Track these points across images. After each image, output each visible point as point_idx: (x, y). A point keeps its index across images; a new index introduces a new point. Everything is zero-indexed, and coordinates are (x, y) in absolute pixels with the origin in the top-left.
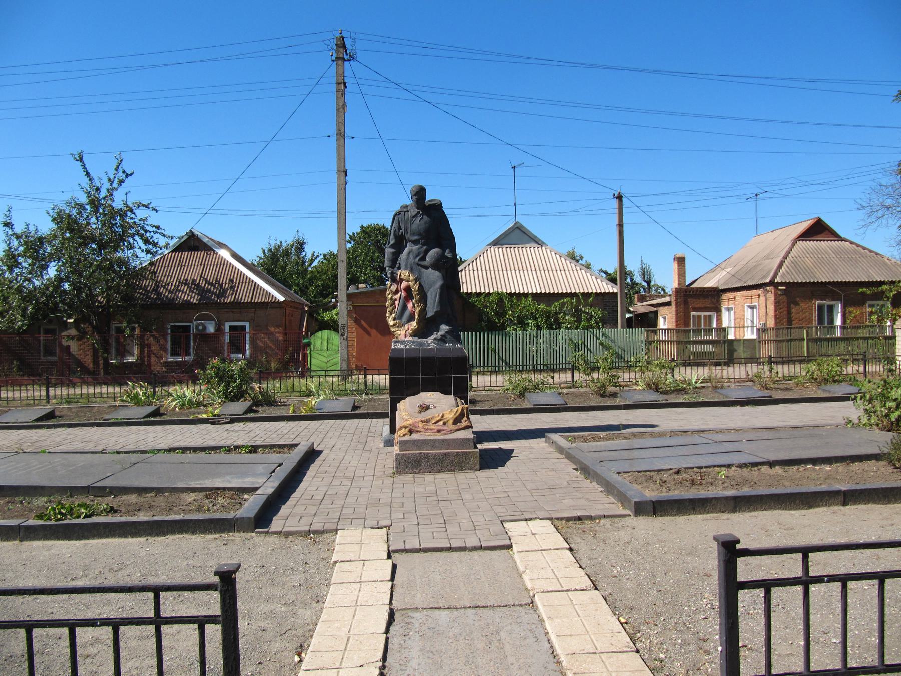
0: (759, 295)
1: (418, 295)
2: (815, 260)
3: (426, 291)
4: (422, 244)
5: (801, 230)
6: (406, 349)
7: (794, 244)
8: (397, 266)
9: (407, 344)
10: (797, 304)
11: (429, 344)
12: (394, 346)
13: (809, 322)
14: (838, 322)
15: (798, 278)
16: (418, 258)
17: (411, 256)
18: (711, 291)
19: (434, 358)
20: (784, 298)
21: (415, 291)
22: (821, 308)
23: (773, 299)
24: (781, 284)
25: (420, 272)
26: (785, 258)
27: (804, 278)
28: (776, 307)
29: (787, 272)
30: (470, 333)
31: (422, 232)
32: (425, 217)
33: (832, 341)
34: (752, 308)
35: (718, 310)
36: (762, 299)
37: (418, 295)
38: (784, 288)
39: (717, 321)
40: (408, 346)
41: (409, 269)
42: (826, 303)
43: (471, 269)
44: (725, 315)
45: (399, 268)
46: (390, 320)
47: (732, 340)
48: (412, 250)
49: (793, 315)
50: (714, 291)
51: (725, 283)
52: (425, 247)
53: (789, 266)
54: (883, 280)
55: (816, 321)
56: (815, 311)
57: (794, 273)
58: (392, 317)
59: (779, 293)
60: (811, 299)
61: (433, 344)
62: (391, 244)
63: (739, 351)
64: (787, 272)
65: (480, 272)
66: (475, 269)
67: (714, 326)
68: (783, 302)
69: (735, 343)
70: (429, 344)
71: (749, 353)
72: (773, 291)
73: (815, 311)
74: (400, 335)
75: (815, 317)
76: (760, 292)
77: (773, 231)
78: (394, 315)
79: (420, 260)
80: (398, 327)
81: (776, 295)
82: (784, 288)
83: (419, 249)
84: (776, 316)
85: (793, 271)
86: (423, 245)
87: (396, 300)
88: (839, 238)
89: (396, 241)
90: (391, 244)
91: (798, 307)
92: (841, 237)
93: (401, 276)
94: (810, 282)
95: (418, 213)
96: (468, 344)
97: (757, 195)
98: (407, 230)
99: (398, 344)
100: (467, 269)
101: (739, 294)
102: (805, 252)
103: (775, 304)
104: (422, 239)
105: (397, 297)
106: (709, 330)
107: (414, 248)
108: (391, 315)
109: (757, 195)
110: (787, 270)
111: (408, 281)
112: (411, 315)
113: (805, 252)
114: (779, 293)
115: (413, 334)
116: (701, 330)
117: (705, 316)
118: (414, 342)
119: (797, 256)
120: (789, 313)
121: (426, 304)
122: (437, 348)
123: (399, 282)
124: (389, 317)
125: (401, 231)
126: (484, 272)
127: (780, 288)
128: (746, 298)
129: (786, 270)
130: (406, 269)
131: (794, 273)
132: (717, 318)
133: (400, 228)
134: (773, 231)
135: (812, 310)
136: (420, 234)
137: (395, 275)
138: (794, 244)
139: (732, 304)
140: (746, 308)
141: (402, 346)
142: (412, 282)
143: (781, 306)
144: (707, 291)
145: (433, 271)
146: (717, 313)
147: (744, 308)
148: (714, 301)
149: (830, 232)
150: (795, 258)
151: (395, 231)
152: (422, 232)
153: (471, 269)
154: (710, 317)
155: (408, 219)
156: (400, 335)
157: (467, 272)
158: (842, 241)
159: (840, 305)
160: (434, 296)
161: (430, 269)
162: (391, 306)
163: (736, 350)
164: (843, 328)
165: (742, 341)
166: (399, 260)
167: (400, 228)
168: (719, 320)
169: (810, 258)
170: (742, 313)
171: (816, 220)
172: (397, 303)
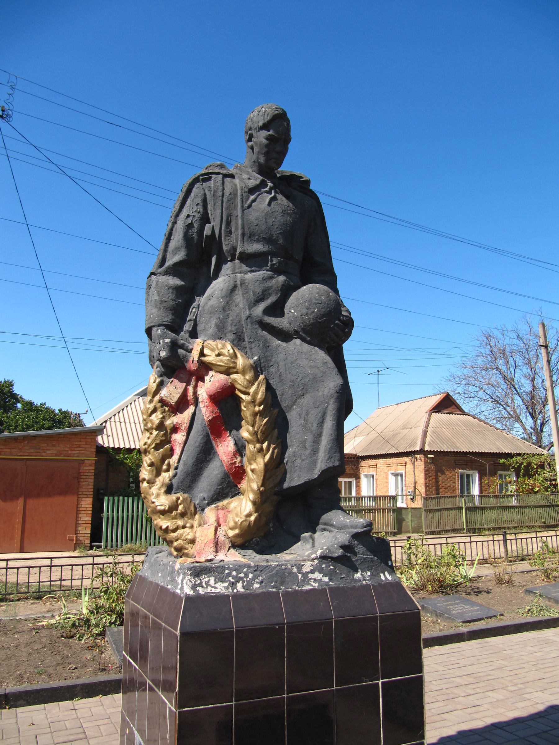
0: (406, 463)
1: (262, 414)
2: (451, 431)
3: (283, 405)
4: (273, 269)
5: (433, 403)
6: (237, 597)
7: (430, 416)
8: (187, 327)
9: (238, 579)
10: (443, 473)
11: (305, 575)
12: (194, 587)
13: (453, 491)
14: (475, 491)
15: (443, 447)
16: (262, 306)
17: (239, 298)
18: (351, 458)
19: (327, 624)
20: (432, 466)
21: (253, 402)
22: (462, 476)
23: (422, 467)
24: (430, 452)
25: (266, 346)
26: (427, 427)
27: (448, 447)
28: (425, 474)
29: (432, 441)
30: (121, 498)
31: (276, 232)
32: (280, 197)
33: (485, 510)
34: (396, 475)
35: (357, 477)
36: (410, 466)
37: (262, 414)
38: (432, 456)
39: (356, 487)
40: (240, 587)
41: (231, 336)
42: (466, 472)
43: (117, 420)
44: (364, 481)
45: (194, 334)
46: (154, 490)
47: (401, 509)
48: (243, 283)
49: (440, 483)
50: (354, 458)
51: (362, 451)
52: (282, 278)
53: (432, 435)
54: (510, 452)
55: (458, 490)
56: (458, 480)
57: (438, 442)
58: (159, 481)
59: (429, 461)
60: (454, 469)
61: (317, 575)
62: (167, 264)
63: (407, 520)
64: (432, 441)
65: (128, 424)
66: (122, 420)
67: (354, 494)
68: (432, 470)
69: (403, 512)
70: (305, 575)
71: (416, 522)
72: (423, 459)
73: (458, 480)
74: (192, 542)
75: (458, 485)
76: (407, 459)
77: (397, 404)
78: (165, 477)
79: (268, 311)
80: (183, 515)
81: (426, 462)
82: (432, 456)
83: (265, 279)
84: (426, 484)
85: (436, 440)
86: (277, 271)
87: (175, 429)
88: (463, 413)
89: (188, 255)
90: (167, 264)
91: (443, 476)
92: (465, 412)
93: (202, 354)
94: (454, 452)
95: (263, 184)
96: (118, 512)
97: (378, 371)
98: (228, 223)
99: (204, 579)
100: (112, 419)
101: (381, 461)
102: (441, 423)
103: (425, 471)
104: (273, 254)
105: (183, 418)
106: (349, 498)
107: (249, 276)
108: (158, 474)
109: (378, 371)
110: (432, 438)
111: (228, 372)
112: (226, 476)
113: (441, 423)
114: (429, 461)
115: (239, 541)
116: (351, 498)
117: (345, 482)
118: (257, 569)
119: (436, 427)
120: (437, 481)
121: (283, 447)
122: (331, 589)
123: (191, 373)
124: (151, 482)
125: (208, 226)
126: (133, 425)
127: (429, 456)
128: (389, 465)
129: (431, 440)
130: (219, 335)
131: (438, 442)
132: (356, 484)
133: (205, 219)
134: (397, 404)
135: (455, 478)
136: (268, 240)
137: (181, 352)
138: (430, 416)
139: (373, 471)
140: (390, 475)
141: (221, 588)
142: (244, 373)
143: (430, 474)
144: (348, 458)
145: (306, 347)
146: (356, 480)
147: (387, 475)
148: (354, 467)
149: (456, 406)
150: (434, 428)
151: (190, 226)
152: (276, 232)
153: (117, 420)
154: (350, 483)
155: (234, 194)
156: (192, 542)
157: (113, 423)
158: (466, 415)
159: (477, 474)
160: (314, 415)
161: (298, 341)
162: (157, 448)
163: (404, 520)
164: (481, 497)
165: (409, 510)
166: (193, 310)
167: (205, 219)
168: (358, 487)
169: (446, 429)
170: (386, 480)
171: (445, 395)
172: (178, 438)
